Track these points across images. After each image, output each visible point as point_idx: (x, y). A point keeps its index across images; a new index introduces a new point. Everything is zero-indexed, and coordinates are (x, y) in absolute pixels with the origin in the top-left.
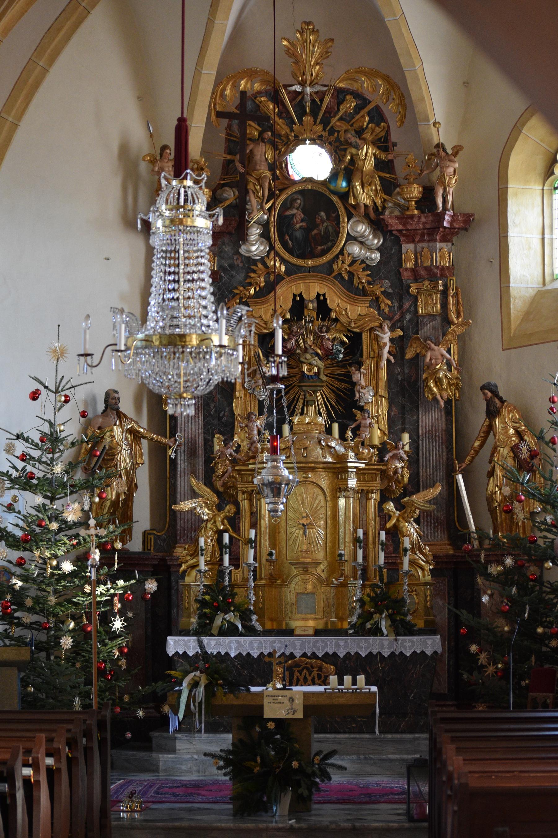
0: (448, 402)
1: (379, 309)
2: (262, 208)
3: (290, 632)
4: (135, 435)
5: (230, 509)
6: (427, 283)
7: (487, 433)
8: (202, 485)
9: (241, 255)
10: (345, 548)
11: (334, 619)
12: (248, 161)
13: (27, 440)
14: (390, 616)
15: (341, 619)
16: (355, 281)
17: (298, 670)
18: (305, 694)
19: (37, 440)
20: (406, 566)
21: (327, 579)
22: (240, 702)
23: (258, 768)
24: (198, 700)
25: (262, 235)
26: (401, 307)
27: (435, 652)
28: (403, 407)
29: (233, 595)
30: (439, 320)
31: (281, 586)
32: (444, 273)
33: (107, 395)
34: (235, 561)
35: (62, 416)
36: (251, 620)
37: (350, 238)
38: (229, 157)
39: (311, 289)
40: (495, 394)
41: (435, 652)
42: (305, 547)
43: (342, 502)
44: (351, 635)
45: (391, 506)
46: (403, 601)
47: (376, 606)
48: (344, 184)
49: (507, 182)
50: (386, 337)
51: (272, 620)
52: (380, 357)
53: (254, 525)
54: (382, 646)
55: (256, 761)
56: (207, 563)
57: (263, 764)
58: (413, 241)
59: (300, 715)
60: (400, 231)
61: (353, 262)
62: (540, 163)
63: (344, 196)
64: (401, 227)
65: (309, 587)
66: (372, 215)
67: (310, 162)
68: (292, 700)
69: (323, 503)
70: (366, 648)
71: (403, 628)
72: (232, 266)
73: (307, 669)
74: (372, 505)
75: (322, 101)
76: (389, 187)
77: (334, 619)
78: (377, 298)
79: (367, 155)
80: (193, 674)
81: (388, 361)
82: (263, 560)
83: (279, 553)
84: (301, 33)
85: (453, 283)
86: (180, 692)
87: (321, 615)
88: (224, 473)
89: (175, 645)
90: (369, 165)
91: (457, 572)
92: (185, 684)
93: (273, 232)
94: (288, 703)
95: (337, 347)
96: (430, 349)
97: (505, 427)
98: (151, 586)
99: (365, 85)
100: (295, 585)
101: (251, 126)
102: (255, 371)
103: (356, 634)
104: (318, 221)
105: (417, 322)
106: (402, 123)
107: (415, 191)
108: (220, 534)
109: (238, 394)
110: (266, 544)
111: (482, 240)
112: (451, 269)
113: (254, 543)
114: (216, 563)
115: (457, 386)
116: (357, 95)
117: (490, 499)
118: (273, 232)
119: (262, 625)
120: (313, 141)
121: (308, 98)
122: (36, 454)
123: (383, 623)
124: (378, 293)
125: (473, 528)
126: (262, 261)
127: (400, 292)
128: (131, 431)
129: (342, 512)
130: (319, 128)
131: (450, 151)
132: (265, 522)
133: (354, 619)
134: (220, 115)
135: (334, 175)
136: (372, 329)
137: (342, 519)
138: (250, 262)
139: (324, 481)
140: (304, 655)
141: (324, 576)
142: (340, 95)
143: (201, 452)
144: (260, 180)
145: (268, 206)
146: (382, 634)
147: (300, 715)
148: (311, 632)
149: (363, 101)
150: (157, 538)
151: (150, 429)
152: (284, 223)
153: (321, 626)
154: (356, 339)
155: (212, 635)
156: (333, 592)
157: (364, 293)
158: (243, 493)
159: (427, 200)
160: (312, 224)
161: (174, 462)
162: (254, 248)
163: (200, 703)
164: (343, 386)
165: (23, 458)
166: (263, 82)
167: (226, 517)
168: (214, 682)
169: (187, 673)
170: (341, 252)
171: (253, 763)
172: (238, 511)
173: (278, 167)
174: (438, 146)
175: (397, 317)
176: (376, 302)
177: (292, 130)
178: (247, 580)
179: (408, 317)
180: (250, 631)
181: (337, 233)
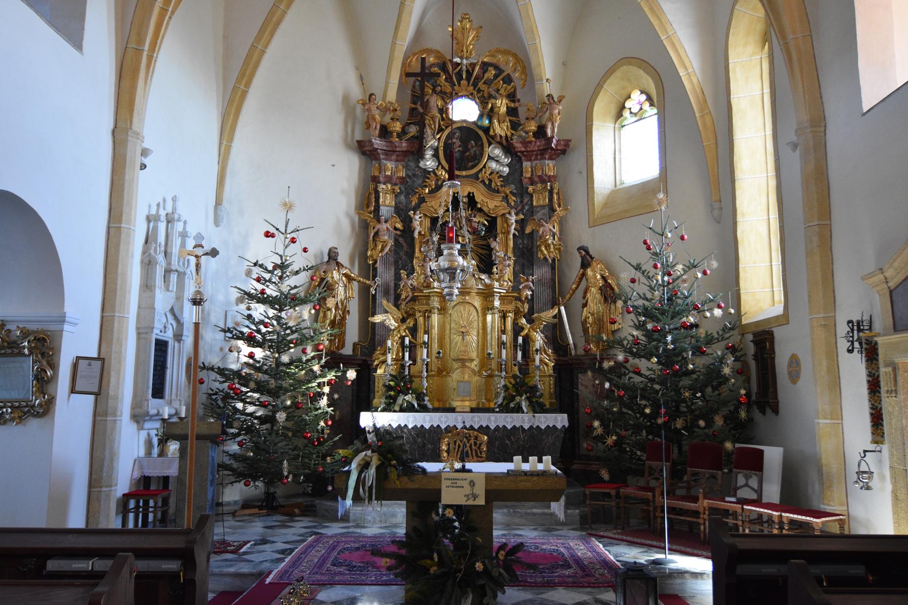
0: (554, 260)
1: (508, 203)
2: (434, 137)
3: (452, 410)
4: (349, 278)
5: (410, 323)
6: (539, 185)
7: (581, 279)
8: (391, 305)
9: (420, 168)
10: (492, 350)
11: (484, 401)
12: (426, 106)
13: (261, 266)
14: (528, 398)
15: (489, 401)
16: (493, 185)
17: (468, 446)
18: (489, 477)
19: (270, 268)
20: (537, 362)
21: (479, 372)
22: (416, 486)
23: (435, 568)
24: (368, 484)
25: (433, 156)
26: (522, 202)
27: (564, 426)
28: (523, 265)
29: (411, 382)
30: (547, 208)
31: (446, 376)
32: (551, 179)
33: (330, 250)
34: (413, 358)
35: (289, 252)
36: (424, 400)
37: (490, 158)
38: (413, 106)
39: (462, 188)
40: (587, 252)
41: (564, 426)
42: (462, 349)
43: (489, 318)
44: (497, 412)
45: (524, 321)
46: (535, 387)
47: (517, 390)
48: (487, 122)
49: (592, 121)
50: (513, 219)
51: (439, 401)
52: (508, 232)
53: (426, 332)
54: (523, 421)
55: (432, 559)
56: (393, 360)
57: (441, 563)
58: (530, 160)
59: (481, 501)
60: (522, 152)
61: (491, 173)
62: (613, 110)
63: (486, 130)
64: (523, 149)
65: (466, 377)
66: (504, 142)
67: (465, 110)
68: (472, 484)
69: (476, 318)
70: (511, 422)
71: (538, 407)
72: (414, 175)
73: (466, 438)
74: (509, 322)
75: (473, 70)
76: (515, 126)
77: (484, 401)
78: (507, 196)
79: (502, 105)
80: (364, 453)
81: (514, 235)
82: (434, 357)
83: (444, 353)
84: (461, 22)
85: (556, 186)
86: (349, 473)
87: (474, 398)
88: (406, 297)
89: (366, 420)
90: (503, 109)
91: (567, 368)
92: (354, 465)
93: (441, 153)
94: (469, 487)
95: (481, 227)
96: (543, 226)
97: (595, 274)
98: (352, 374)
99: (500, 59)
100: (456, 376)
101: (429, 80)
102: (428, 240)
103: (501, 412)
104: (470, 146)
105: (532, 211)
106: (524, 85)
107: (533, 127)
108: (402, 338)
109: (417, 255)
110: (435, 346)
111: (575, 159)
112: (555, 177)
113: (426, 345)
114: (399, 360)
115: (559, 250)
116: (496, 67)
117: (584, 323)
118: (441, 153)
119: (432, 404)
120: (467, 96)
121: (464, 67)
122: (267, 276)
123: (523, 403)
124: (508, 192)
125: (571, 342)
126: (434, 172)
127: (522, 192)
128: (346, 275)
129: (489, 325)
130: (471, 88)
131: (556, 100)
132: (435, 331)
133: (500, 401)
134: (408, 75)
135: (481, 116)
136: (504, 215)
137: (489, 329)
138: (426, 172)
139: (477, 302)
140: (465, 427)
141: (476, 369)
142: (485, 66)
143: (392, 292)
144: (433, 118)
145: (438, 136)
146: (523, 412)
147: (481, 501)
148: (468, 410)
149: (499, 70)
150: (362, 347)
151: (360, 275)
152: (448, 147)
153: (474, 405)
154: (493, 221)
155: (395, 411)
156: (483, 380)
157: (498, 192)
158: (420, 312)
159: (541, 132)
160: (466, 149)
161: (374, 296)
162: (428, 163)
163: (371, 488)
164: (484, 252)
165: (258, 280)
166: (436, 57)
167: (407, 328)
168: (387, 463)
169: (357, 452)
170: (484, 167)
171: (429, 562)
172: (415, 325)
173: (443, 111)
174: (549, 95)
175: (519, 208)
176: (506, 198)
177: (453, 89)
178: (422, 372)
179: (527, 208)
180: (423, 409)
181: (482, 155)
